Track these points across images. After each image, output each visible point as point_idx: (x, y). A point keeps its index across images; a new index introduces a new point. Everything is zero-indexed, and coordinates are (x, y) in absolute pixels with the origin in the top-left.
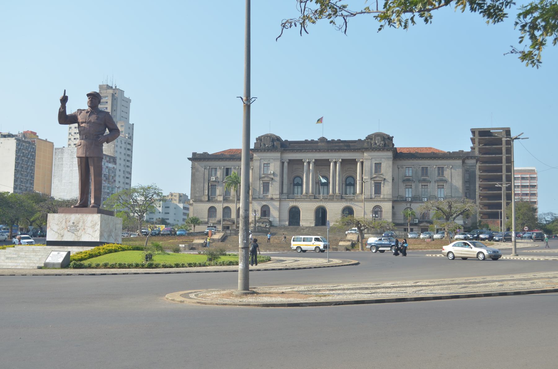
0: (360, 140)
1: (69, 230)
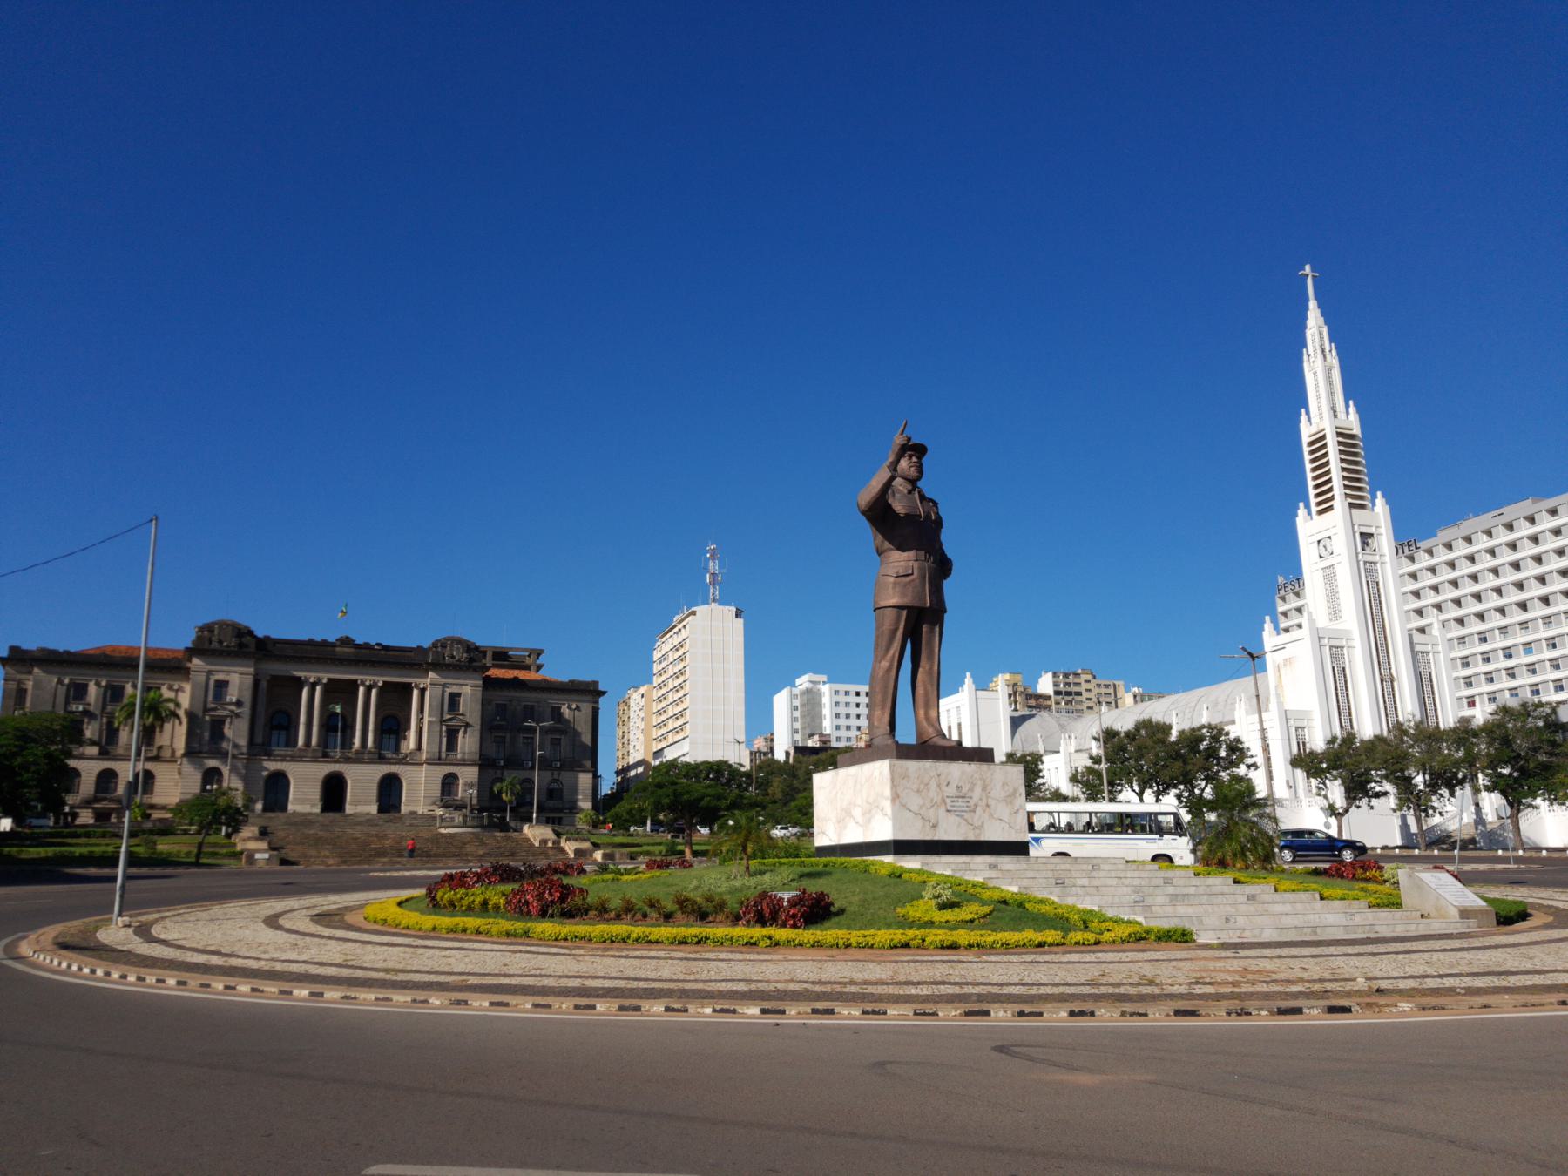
0: (420, 648)
1: (949, 808)
